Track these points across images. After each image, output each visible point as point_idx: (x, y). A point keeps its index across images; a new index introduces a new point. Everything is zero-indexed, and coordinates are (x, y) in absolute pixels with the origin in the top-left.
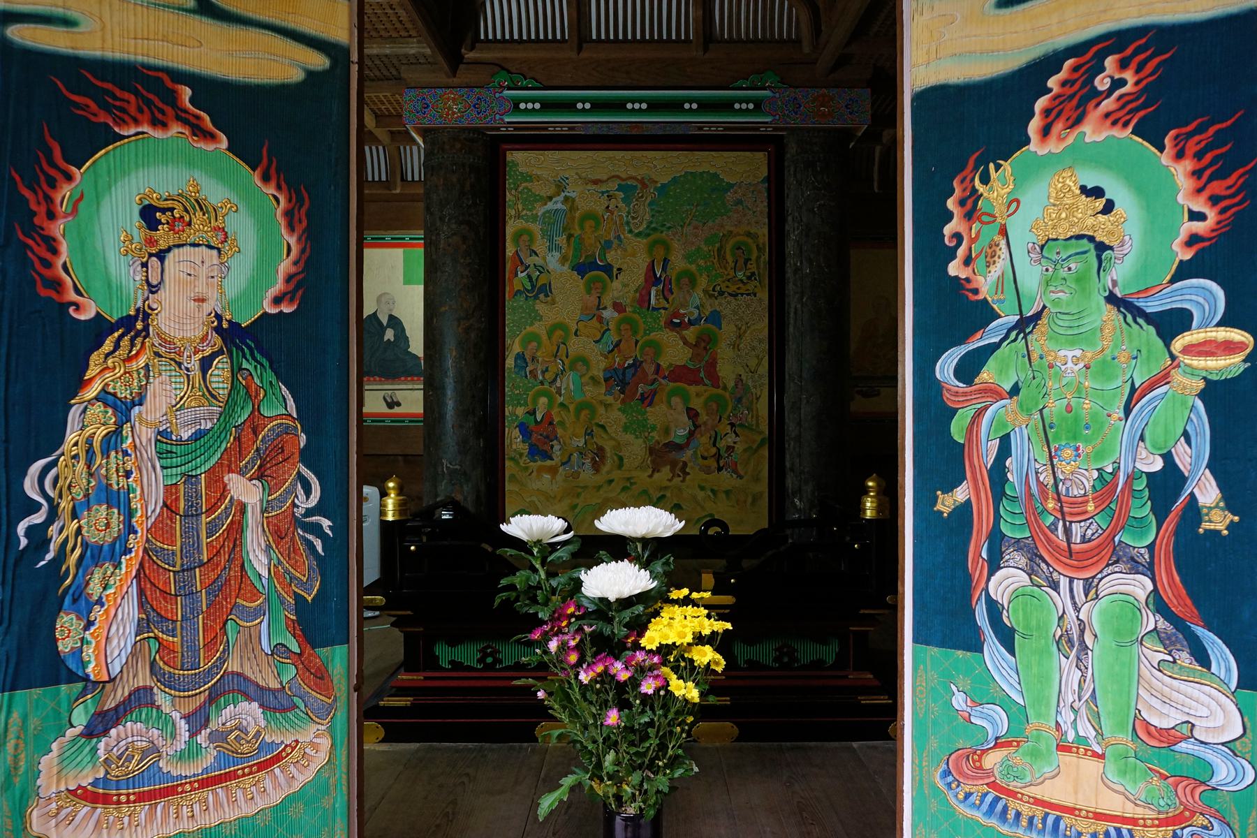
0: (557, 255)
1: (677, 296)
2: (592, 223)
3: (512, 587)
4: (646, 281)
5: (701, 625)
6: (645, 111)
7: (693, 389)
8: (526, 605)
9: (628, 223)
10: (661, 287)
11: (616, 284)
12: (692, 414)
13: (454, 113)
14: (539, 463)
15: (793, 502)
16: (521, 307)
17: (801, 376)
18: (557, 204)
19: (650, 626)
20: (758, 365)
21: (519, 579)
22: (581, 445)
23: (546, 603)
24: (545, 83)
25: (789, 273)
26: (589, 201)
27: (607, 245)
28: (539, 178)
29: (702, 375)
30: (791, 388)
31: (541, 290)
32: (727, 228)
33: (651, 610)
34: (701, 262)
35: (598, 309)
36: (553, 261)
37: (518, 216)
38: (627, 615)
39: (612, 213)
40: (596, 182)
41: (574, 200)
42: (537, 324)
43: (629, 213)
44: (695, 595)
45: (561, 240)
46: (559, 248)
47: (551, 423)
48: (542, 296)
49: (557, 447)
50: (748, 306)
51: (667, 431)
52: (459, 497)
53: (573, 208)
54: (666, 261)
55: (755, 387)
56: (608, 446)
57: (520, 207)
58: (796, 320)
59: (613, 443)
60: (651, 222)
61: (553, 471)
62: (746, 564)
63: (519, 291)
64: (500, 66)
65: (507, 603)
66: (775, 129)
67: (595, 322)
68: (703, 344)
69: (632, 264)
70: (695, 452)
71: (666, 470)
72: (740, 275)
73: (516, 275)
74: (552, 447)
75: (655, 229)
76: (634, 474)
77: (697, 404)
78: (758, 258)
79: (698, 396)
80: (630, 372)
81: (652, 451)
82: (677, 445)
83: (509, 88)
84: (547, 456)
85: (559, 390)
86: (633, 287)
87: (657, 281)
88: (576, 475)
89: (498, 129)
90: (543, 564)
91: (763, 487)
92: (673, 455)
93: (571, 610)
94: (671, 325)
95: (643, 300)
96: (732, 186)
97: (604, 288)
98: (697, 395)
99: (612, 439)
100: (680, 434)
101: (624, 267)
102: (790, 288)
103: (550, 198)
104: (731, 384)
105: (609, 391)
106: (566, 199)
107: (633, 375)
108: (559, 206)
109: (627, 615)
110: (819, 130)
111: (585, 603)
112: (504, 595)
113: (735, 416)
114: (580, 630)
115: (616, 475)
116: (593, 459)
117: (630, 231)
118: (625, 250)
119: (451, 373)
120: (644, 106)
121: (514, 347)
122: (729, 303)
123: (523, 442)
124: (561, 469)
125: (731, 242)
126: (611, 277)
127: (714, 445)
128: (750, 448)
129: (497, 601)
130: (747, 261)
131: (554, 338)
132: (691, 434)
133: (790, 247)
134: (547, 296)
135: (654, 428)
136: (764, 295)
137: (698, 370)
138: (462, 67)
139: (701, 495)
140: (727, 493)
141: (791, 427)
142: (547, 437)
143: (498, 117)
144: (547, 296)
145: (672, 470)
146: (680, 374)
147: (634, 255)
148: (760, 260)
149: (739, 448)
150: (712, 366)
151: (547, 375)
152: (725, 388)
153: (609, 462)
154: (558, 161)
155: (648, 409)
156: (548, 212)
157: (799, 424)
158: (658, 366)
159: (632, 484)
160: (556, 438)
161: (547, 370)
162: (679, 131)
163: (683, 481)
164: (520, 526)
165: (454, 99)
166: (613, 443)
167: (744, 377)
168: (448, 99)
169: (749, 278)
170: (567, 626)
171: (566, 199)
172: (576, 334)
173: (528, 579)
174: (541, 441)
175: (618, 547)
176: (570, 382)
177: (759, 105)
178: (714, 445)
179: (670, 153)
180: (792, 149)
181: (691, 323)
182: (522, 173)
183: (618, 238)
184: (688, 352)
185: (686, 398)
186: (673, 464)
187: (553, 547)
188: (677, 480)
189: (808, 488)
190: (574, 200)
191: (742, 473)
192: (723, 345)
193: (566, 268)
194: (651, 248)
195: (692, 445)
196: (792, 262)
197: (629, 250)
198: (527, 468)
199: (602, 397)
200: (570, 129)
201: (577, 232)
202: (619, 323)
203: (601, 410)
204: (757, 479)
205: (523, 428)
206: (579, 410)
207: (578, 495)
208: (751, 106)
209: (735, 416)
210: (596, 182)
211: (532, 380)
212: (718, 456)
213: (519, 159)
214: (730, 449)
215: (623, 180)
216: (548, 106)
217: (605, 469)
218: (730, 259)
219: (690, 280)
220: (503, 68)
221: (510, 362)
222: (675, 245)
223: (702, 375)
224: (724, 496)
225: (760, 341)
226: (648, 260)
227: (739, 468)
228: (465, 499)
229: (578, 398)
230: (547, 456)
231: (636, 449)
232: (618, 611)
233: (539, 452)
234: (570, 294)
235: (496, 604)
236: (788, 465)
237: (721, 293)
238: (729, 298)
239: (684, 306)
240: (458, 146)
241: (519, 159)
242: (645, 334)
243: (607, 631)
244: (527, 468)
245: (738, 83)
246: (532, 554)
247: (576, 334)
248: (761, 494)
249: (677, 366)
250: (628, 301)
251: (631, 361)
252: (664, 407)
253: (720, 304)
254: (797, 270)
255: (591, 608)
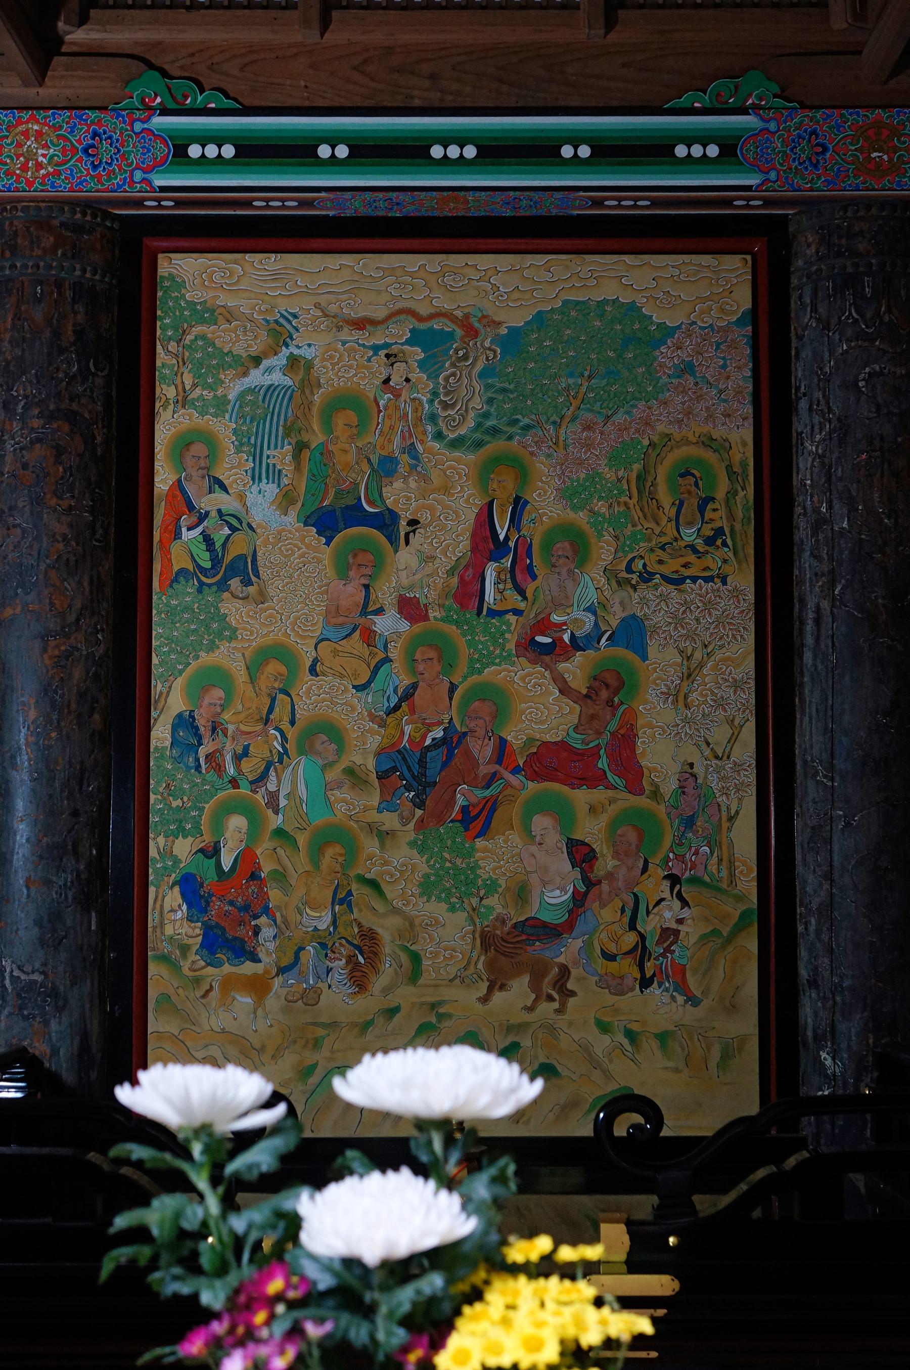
0: (271, 489)
1: (544, 584)
2: (352, 417)
3: (140, 1234)
4: (474, 548)
5: (579, 1323)
6: (470, 163)
7: (582, 797)
8: (176, 1278)
9: (433, 418)
10: (508, 562)
11: (405, 557)
12: (581, 854)
13: (39, 166)
14: (227, 968)
15: (817, 1060)
16: (187, 609)
17: (831, 767)
18: (271, 374)
19: (460, 1323)
20: (733, 739)
21: (159, 1213)
22: (322, 926)
23: (222, 1270)
24: (247, 102)
25: (802, 530)
26: (344, 368)
27: (386, 468)
28: (230, 316)
29: (603, 763)
30: (809, 795)
31: (232, 569)
32: (660, 428)
33: (463, 1287)
34: (601, 506)
35: (364, 612)
36: (260, 502)
37: (183, 401)
38: (405, 1297)
39: (397, 396)
40: (360, 324)
41: (309, 365)
42: (224, 647)
43: (435, 394)
44: (567, 1254)
45: (281, 456)
46: (275, 475)
47: (254, 876)
48: (235, 583)
49: (267, 932)
50: (708, 606)
51: (522, 894)
52: (40, 1048)
53: (308, 384)
54: (519, 505)
55: (725, 792)
56: (387, 930)
57: (188, 381)
58: (817, 640)
59: (394, 921)
60: (486, 415)
61: (258, 987)
62: (706, 1204)
63: (183, 572)
64: (144, 61)
65: (133, 1276)
66: (768, 203)
67: (356, 643)
68: (604, 694)
69: (444, 510)
70: (588, 944)
71: (520, 989)
72: (689, 534)
73: (177, 535)
74: (257, 931)
75: (494, 432)
76: (448, 993)
77: (591, 830)
78: (732, 494)
79: (594, 813)
80: (436, 758)
81: (487, 941)
82: (545, 925)
83: (165, 112)
84: (244, 951)
85: (273, 799)
86: (443, 563)
87: (499, 549)
88: (311, 997)
89: (139, 203)
90: (215, 1181)
91: (747, 1025)
92: (537, 949)
93: (275, 1286)
94: (530, 648)
95: (468, 593)
96: (670, 332)
97: (378, 566)
98: (593, 810)
99: (396, 911)
100: (552, 900)
101: (424, 517)
102: (806, 564)
103: (257, 361)
104: (669, 787)
105: (386, 804)
106: (293, 362)
107: (445, 764)
108: (277, 378)
109: (405, 1297)
110: (868, 204)
111: (312, 1271)
112: (123, 1253)
113: (680, 858)
114: (295, 1332)
115: (406, 995)
116: (351, 959)
117: (439, 436)
118: (426, 479)
119: (24, 760)
120: (470, 152)
121: (171, 699)
122: (664, 598)
123: (190, 919)
124: (277, 982)
125: (672, 458)
126: (393, 540)
127: (632, 926)
128: (715, 932)
129: (107, 1267)
130: (705, 502)
131: (264, 684)
132: (579, 901)
133: (805, 470)
134: (247, 583)
135: (491, 887)
136: (744, 581)
137: (594, 754)
138: (57, 60)
139: (601, 1044)
140: (663, 1038)
141: (810, 884)
142: (246, 908)
143: (138, 175)
144: (247, 583)
145: (535, 986)
146: (553, 763)
147: (446, 490)
148: (736, 503)
149: (691, 933)
150: (624, 746)
151: (247, 765)
152: (656, 795)
153: (387, 968)
154: (276, 277)
155: (480, 843)
156: (251, 390)
157: (829, 877)
158: (502, 744)
159: (441, 1017)
160: (267, 911)
161: (246, 753)
162: (550, 207)
163: (560, 1011)
164: (163, 1092)
165: (39, 134)
166: (394, 921)
167: (699, 769)
168: (26, 134)
169: (710, 541)
170: (268, 1322)
171: (293, 362)
172: (313, 671)
173: (178, 1215)
174: (230, 918)
175: (392, 1147)
176: (299, 779)
177: (729, 149)
178: (632, 926)
179: (530, 259)
180: (807, 248)
181: (576, 645)
182: (191, 304)
183: (411, 450)
184: (571, 712)
185: (563, 816)
186: (538, 973)
187: (245, 1140)
188: (546, 1009)
189: (851, 1028)
190: (309, 365)
191: (698, 993)
192: (652, 694)
193: (291, 518)
194: (486, 472)
195: (580, 927)
196: (809, 501)
197: (436, 479)
198: (197, 981)
199: (373, 816)
200: (303, 204)
201: (317, 438)
202: (413, 645)
203: (371, 846)
204: (732, 1008)
205: (189, 886)
206: (318, 848)
207: (316, 1044)
208: (713, 151)
209: (680, 858)
210: (360, 324)
211: (211, 776)
212: (640, 952)
213: (188, 274)
214: (669, 935)
215: (421, 319)
216: (252, 151)
217: (379, 983)
218: (666, 499)
219: (575, 546)
220: (151, 66)
221: (161, 734)
222: (541, 466)
223: (603, 763)
224: (655, 1044)
225: (736, 686)
226: (480, 502)
227: (691, 980)
228: (55, 1052)
229: (319, 817)
230: (244, 951)
231: (450, 934)
232: (386, 1288)
233: (226, 941)
234: (299, 578)
235: (147, 1357)
236: (804, 973)
237: (646, 577)
238: (665, 588)
239: (561, 604)
240: (48, 241)
241: (188, 274)
242: (473, 671)
243: (359, 1334)
244: (197, 981)
245: (684, 101)
246: (189, 1157)
247: (313, 671)
248: (743, 1040)
249: (545, 744)
250: (433, 595)
251: (438, 733)
252: (515, 838)
253: (644, 601)
254: (819, 523)
255: (325, 1281)
